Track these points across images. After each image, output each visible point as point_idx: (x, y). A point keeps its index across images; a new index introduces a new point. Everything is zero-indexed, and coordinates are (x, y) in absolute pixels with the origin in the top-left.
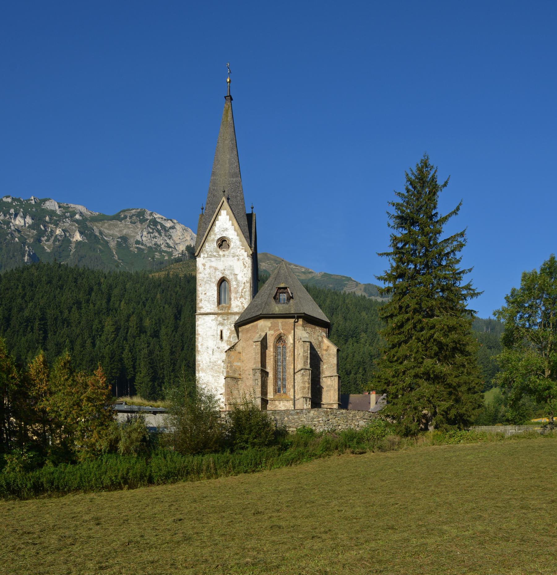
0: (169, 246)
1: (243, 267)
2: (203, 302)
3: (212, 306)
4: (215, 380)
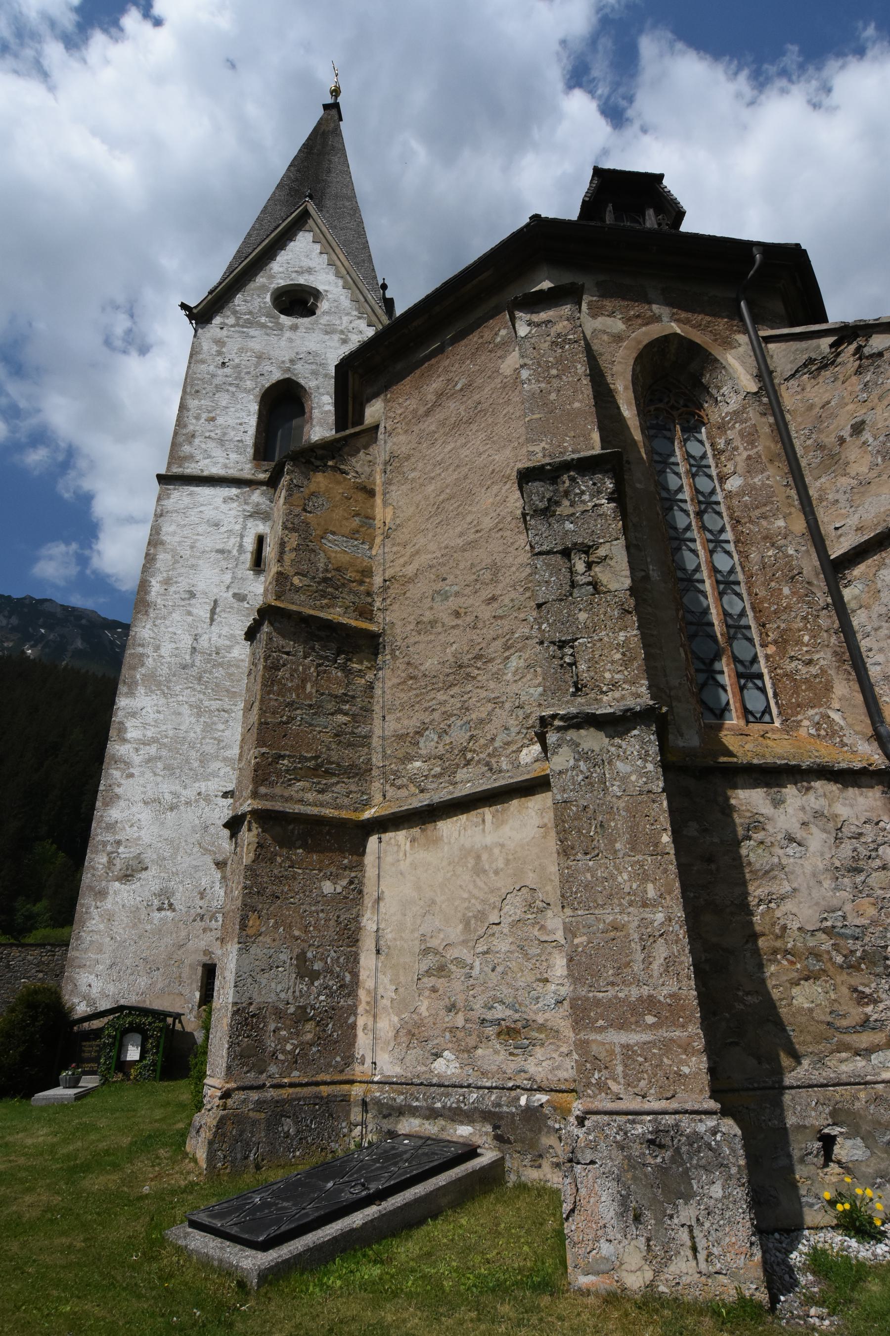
2: (197, 441)
3: (233, 456)
4: (208, 728)
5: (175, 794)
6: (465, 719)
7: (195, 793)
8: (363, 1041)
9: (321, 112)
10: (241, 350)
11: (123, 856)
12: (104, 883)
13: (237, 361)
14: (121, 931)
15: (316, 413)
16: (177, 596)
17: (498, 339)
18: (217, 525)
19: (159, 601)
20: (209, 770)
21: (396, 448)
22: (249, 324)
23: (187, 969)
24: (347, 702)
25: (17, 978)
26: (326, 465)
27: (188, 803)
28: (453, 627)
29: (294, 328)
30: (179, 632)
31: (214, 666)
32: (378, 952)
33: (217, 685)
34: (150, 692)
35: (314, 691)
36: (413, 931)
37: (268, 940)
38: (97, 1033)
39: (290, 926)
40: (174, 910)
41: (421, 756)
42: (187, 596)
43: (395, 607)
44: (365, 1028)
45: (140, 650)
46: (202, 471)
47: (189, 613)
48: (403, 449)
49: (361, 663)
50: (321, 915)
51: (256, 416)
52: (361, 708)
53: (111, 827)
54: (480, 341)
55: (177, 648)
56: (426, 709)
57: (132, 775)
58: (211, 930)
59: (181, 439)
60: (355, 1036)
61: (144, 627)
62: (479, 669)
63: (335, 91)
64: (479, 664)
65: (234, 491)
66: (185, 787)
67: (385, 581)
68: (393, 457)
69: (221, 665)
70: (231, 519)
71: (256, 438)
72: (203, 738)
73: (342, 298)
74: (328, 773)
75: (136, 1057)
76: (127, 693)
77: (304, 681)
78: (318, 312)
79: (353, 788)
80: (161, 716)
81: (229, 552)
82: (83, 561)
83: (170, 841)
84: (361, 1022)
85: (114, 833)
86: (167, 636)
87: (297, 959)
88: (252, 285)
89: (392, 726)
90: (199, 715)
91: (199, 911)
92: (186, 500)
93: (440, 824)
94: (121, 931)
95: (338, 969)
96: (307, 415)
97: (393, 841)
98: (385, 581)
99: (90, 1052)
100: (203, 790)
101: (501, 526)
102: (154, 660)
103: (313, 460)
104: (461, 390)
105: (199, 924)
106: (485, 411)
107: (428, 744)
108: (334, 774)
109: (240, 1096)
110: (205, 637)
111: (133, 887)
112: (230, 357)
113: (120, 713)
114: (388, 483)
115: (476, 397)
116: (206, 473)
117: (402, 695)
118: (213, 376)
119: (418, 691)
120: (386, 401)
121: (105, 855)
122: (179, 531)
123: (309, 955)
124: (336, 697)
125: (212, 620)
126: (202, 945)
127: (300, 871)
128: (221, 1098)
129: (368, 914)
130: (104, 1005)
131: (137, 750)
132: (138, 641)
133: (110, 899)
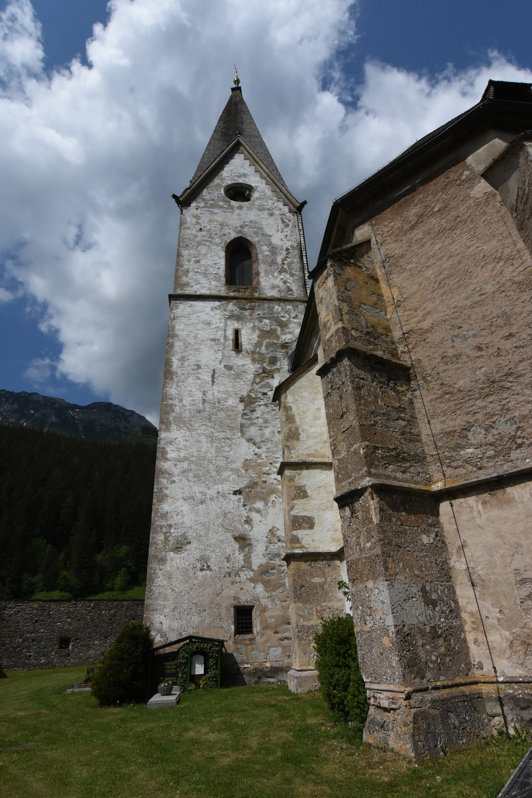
0: (126, 428)
1: (281, 226)
2: (190, 274)
3: (213, 283)
4: (219, 450)
5: (202, 493)
6: (508, 417)
7: (216, 492)
8: (476, 653)
9: (230, 93)
10: (210, 221)
11: (174, 535)
12: (163, 553)
13: (208, 227)
14: (178, 585)
15: (260, 256)
16: (189, 368)
17: (464, 177)
18: (209, 324)
19: (178, 371)
20: (223, 477)
21: (389, 252)
22: (213, 206)
23: (224, 610)
24: (402, 412)
25: (55, 623)
26: (350, 262)
27: (212, 499)
28: (478, 357)
29: (240, 208)
30: (194, 390)
31: (218, 411)
32: (473, 585)
33: (221, 422)
34: (179, 428)
35: (383, 404)
36: (505, 567)
37: (402, 577)
38: (174, 656)
39: (412, 568)
40: (211, 570)
41: (472, 445)
42: (196, 368)
43: (418, 349)
44: (476, 641)
45: (171, 402)
46: (195, 292)
47: (198, 378)
48: (397, 251)
49: (402, 387)
50: (426, 559)
51: (224, 259)
52: (411, 416)
53: (164, 516)
54: (447, 180)
55: (193, 400)
56: (467, 413)
57: (174, 482)
58: (237, 583)
59: (180, 273)
60: (468, 648)
61: (171, 387)
62: (511, 382)
63: (236, 81)
64: (511, 379)
65: (217, 303)
66: (209, 489)
67: (404, 334)
68: (388, 257)
69: (222, 410)
70: (217, 320)
71: (226, 272)
72: (217, 457)
73: (266, 190)
74: (404, 460)
75: (202, 672)
76: (165, 429)
77: (376, 397)
78: (252, 199)
79: (420, 470)
80: (188, 443)
81: (219, 340)
82: (54, 369)
83: (203, 524)
84: (470, 637)
85: (167, 520)
86: (186, 393)
87: (422, 591)
88: (212, 184)
89: (437, 426)
90: (212, 442)
91: (227, 570)
92: (188, 310)
93: (509, 490)
94: (178, 585)
95: (446, 598)
96: (254, 258)
97: (464, 504)
98: (404, 334)
99: (170, 669)
100: (220, 490)
101: (503, 289)
102: (180, 408)
103: (343, 259)
104: (439, 211)
105: (228, 579)
106: (465, 221)
107: (477, 435)
108: (407, 461)
109: (417, 697)
110: (210, 393)
111: (183, 555)
112: (204, 225)
113: (162, 442)
114: (388, 274)
115: (454, 214)
116: (198, 293)
117: (442, 405)
118: (196, 236)
119: (457, 402)
120: (372, 225)
121: (162, 535)
122: (186, 328)
123: (428, 588)
124: (396, 408)
125: (213, 382)
126: (232, 593)
127: (407, 528)
128: (406, 699)
129: (454, 558)
130: (173, 637)
131: (175, 465)
132: (169, 396)
133: (168, 563)
